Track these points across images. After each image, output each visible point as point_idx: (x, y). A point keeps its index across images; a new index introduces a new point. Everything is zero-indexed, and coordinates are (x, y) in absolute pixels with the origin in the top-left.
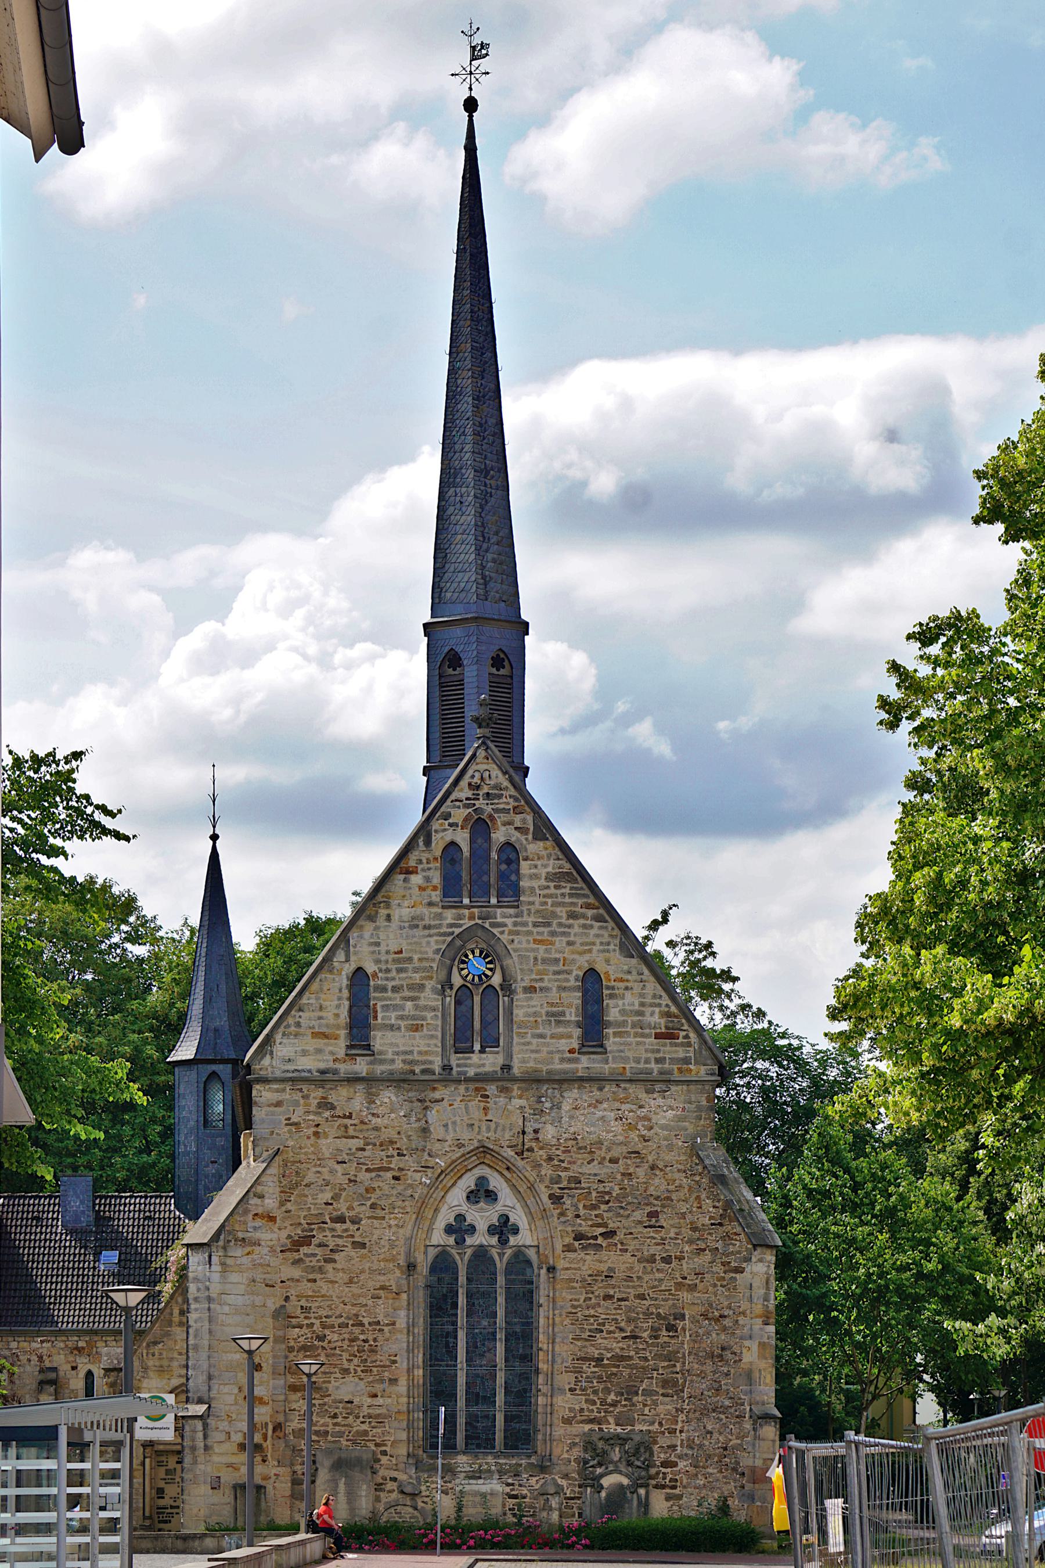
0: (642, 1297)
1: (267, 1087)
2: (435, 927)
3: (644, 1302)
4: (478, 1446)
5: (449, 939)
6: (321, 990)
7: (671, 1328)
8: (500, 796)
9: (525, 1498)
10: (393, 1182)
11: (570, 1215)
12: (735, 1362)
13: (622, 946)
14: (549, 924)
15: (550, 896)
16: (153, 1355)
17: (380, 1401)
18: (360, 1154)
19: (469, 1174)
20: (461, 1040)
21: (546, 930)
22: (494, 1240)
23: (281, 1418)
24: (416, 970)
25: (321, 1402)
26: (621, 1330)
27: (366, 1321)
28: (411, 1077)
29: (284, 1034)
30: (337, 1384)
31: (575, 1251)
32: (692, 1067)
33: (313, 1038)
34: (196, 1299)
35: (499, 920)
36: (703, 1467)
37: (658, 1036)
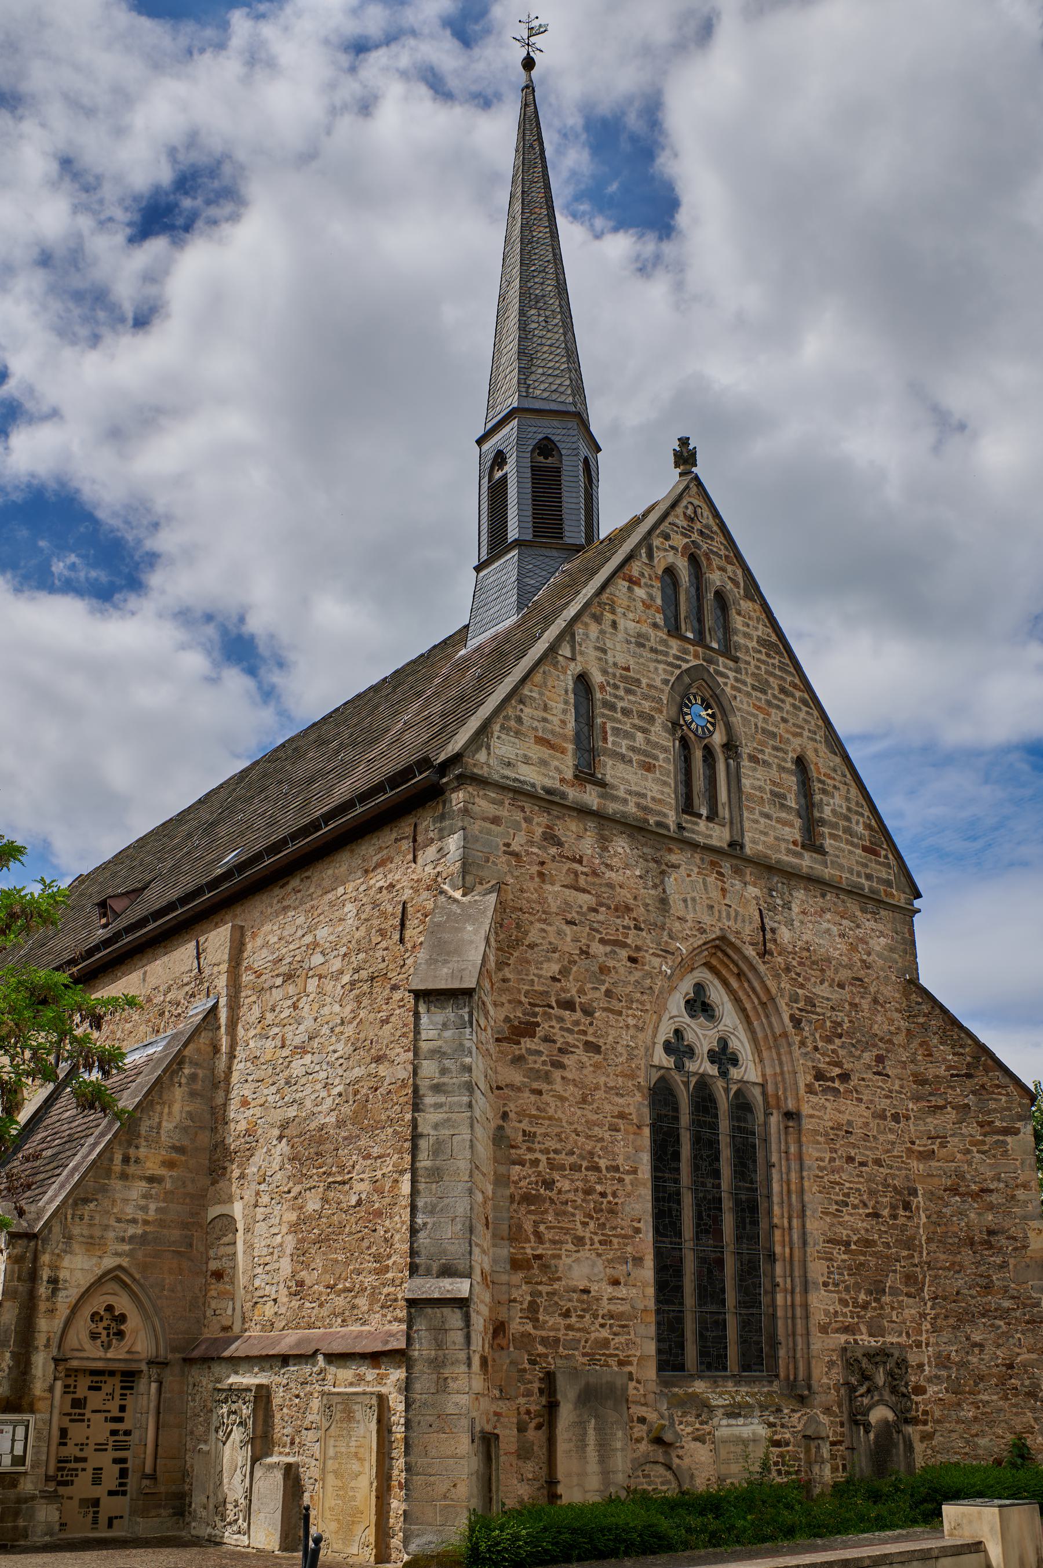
1: (481, 793)
2: (661, 652)
3: (881, 1170)
5: (677, 672)
6: (545, 683)
9: (787, 1444)
10: (629, 964)
12: (1015, 1249)
16: (81, 1219)
17: (622, 1292)
18: (592, 916)
24: (645, 697)
25: (549, 1288)
26: (865, 1205)
27: (603, 1163)
29: (502, 727)
30: (569, 1261)
31: (816, 1094)
33: (536, 743)
34: (437, 1088)
35: (721, 669)
36: (970, 1393)
37: (865, 849)
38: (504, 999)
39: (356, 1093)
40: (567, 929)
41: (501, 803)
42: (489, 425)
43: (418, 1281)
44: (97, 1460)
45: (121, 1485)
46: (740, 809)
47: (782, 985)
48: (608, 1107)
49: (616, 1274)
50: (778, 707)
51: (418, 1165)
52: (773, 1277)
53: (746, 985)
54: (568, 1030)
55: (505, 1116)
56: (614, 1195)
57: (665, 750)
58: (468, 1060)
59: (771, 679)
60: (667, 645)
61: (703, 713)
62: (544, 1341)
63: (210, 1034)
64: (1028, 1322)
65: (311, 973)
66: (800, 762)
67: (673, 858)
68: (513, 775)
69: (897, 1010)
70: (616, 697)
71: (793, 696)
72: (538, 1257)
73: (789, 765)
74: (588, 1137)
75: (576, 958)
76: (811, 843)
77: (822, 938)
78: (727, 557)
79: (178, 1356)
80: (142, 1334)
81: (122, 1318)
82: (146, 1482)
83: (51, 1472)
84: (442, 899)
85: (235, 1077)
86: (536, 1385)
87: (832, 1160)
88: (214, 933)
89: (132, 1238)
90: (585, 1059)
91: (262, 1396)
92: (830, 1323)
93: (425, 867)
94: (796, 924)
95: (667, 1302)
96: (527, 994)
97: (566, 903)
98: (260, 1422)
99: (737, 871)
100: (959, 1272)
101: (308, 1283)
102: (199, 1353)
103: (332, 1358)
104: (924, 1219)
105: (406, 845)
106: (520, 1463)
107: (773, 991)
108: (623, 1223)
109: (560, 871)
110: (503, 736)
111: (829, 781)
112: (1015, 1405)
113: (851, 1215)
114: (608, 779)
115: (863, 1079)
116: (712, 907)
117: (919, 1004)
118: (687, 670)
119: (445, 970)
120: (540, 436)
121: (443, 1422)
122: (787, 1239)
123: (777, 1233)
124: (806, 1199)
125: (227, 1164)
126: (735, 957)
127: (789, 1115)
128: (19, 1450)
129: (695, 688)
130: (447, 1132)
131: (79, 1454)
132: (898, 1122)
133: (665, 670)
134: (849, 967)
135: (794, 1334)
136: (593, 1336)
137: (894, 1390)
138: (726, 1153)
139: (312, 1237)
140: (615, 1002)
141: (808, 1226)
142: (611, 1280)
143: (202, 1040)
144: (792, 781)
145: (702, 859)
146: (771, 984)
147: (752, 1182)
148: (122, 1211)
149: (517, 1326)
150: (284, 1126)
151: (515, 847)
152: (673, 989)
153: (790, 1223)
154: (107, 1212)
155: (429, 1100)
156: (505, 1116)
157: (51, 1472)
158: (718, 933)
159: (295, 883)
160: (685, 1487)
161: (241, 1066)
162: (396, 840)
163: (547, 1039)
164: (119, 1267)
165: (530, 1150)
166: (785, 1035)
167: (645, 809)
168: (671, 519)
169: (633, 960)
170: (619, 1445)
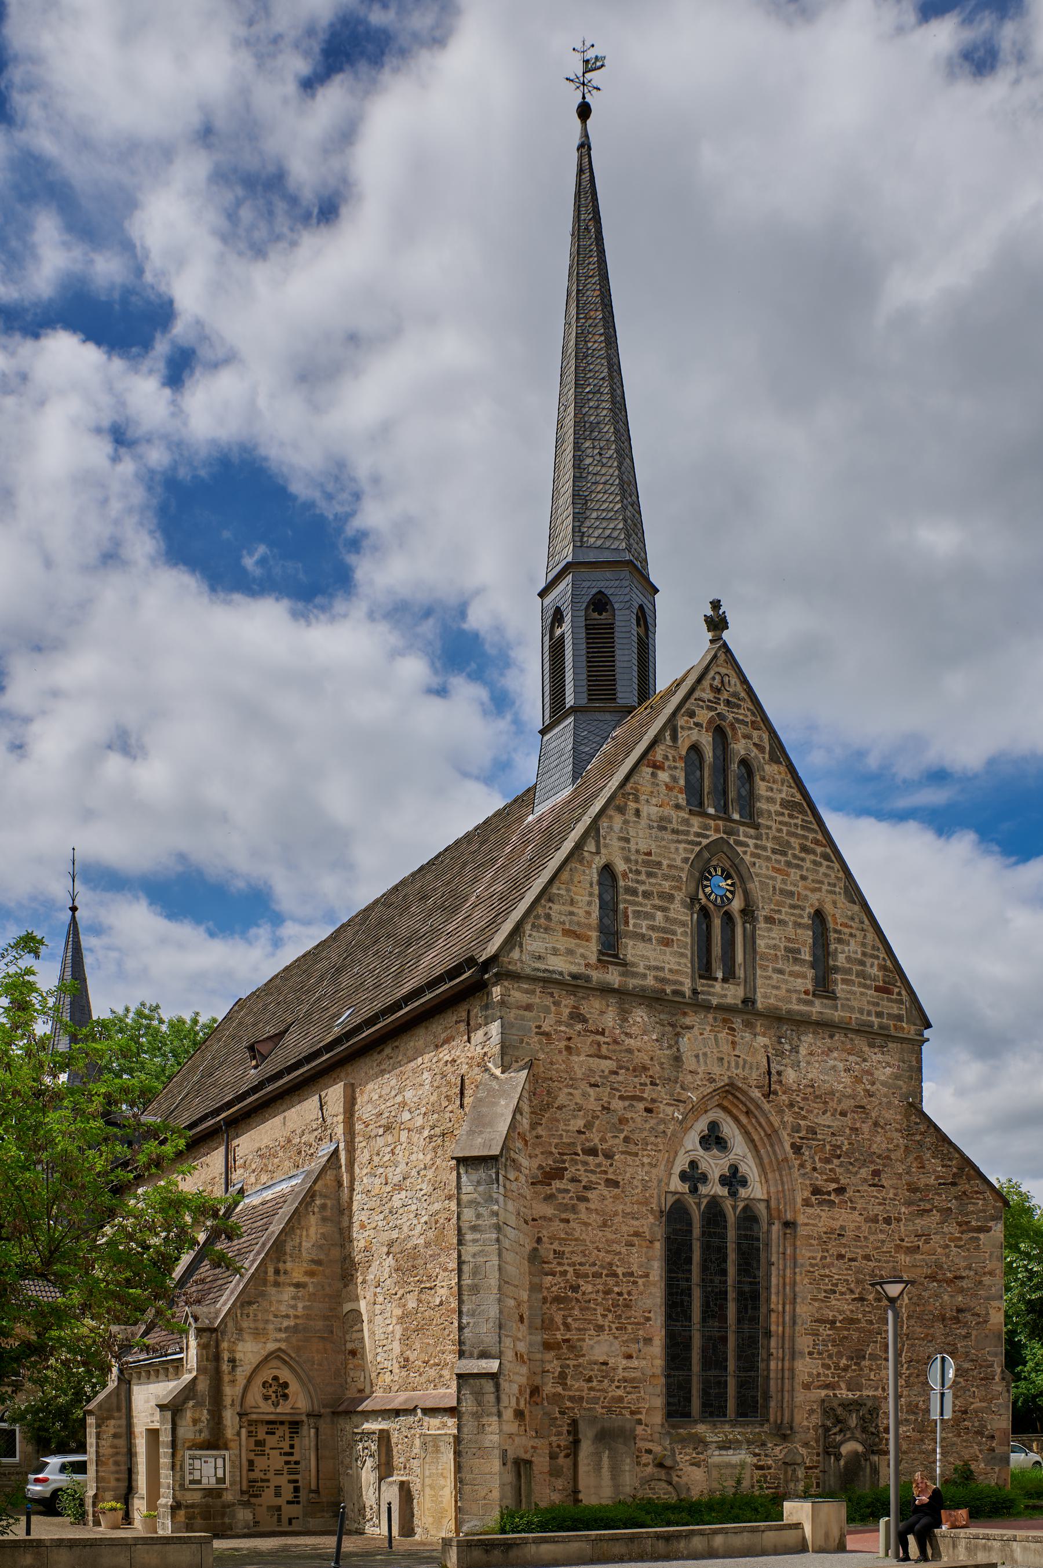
1: (516, 986)
3: (870, 1263)
5: (697, 849)
9: (769, 1468)
10: (645, 1114)
12: (978, 1323)
16: (248, 1316)
17: (635, 1363)
24: (666, 877)
25: (575, 1362)
26: (852, 1292)
27: (620, 1271)
29: (533, 926)
30: (591, 1342)
31: (812, 1206)
32: (905, 1025)
33: (564, 935)
34: (474, 1228)
35: (742, 838)
37: (878, 989)
38: (538, 1151)
39: (436, 1222)
40: (591, 1091)
41: (533, 992)
42: (550, 577)
43: (464, 1362)
45: (295, 1497)
46: (754, 968)
47: (785, 1119)
48: (624, 1228)
49: (629, 1351)
50: (798, 867)
51: (462, 1283)
52: (769, 1349)
53: (754, 1121)
55: (539, 1240)
56: (629, 1293)
57: (683, 924)
58: (496, 1207)
59: (792, 840)
61: (723, 884)
62: (571, 1399)
63: (335, 1172)
64: (982, 1379)
65: (402, 1127)
66: (819, 916)
67: (688, 1021)
68: (543, 967)
69: (897, 1130)
70: (638, 882)
71: (814, 853)
72: (567, 1341)
73: (806, 920)
74: (608, 1252)
75: (599, 1113)
76: (823, 987)
77: (827, 1074)
78: (753, 722)
79: (328, 1410)
80: (301, 1396)
81: (285, 1385)
82: (312, 1495)
83: (244, 1488)
84: (487, 1076)
85: (355, 1207)
86: (565, 1428)
87: (823, 1258)
88: (331, 1089)
89: (287, 1328)
90: (605, 1193)
91: (384, 1437)
92: (813, 1382)
93: (475, 1050)
94: (803, 1064)
95: (677, 1369)
96: (556, 1146)
97: (590, 1070)
98: (383, 1455)
99: (748, 1025)
100: (931, 1341)
101: (411, 1359)
102: (342, 1406)
103: (426, 1411)
104: (906, 1301)
105: (462, 1027)
106: (553, 1479)
107: (776, 1125)
108: (636, 1314)
109: (585, 1044)
110: (534, 934)
111: (846, 930)
112: (965, 1441)
113: (838, 1300)
114: (629, 958)
115: (858, 1191)
116: (722, 1059)
117: (917, 1124)
118: (707, 846)
119: (480, 1140)
120: (594, 591)
121: (482, 1451)
122: (781, 1320)
123: (773, 1316)
124: (797, 1289)
125: (354, 1272)
126: (744, 1099)
127: (787, 1224)
128: (220, 1474)
129: (714, 860)
130: (482, 1260)
131: (264, 1477)
132: (889, 1224)
133: (685, 849)
134: (853, 1097)
135: (782, 1391)
136: (610, 1394)
137: (864, 1430)
138: (732, 1256)
139: (413, 1327)
140: (632, 1146)
141: (798, 1310)
142: (629, 1357)
143: (328, 1177)
144: (807, 936)
145: (715, 1019)
146: (775, 1120)
147: (755, 1278)
148: (278, 1309)
149: (549, 1388)
150: (390, 1245)
151: (546, 1028)
152: (686, 1130)
153: (784, 1308)
154: (267, 1311)
155: (469, 1237)
156: (539, 1240)
157: (244, 1488)
158: (727, 1081)
159: (388, 1051)
160: (682, 1497)
161: (359, 1197)
162: (457, 1022)
163: (574, 1180)
164: (280, 1349)
165: (559, 1264)
166: (785, 1160)
167: (663, 980)
168: (697, 694)
169: (648, 1110)
170: (627, 1468)
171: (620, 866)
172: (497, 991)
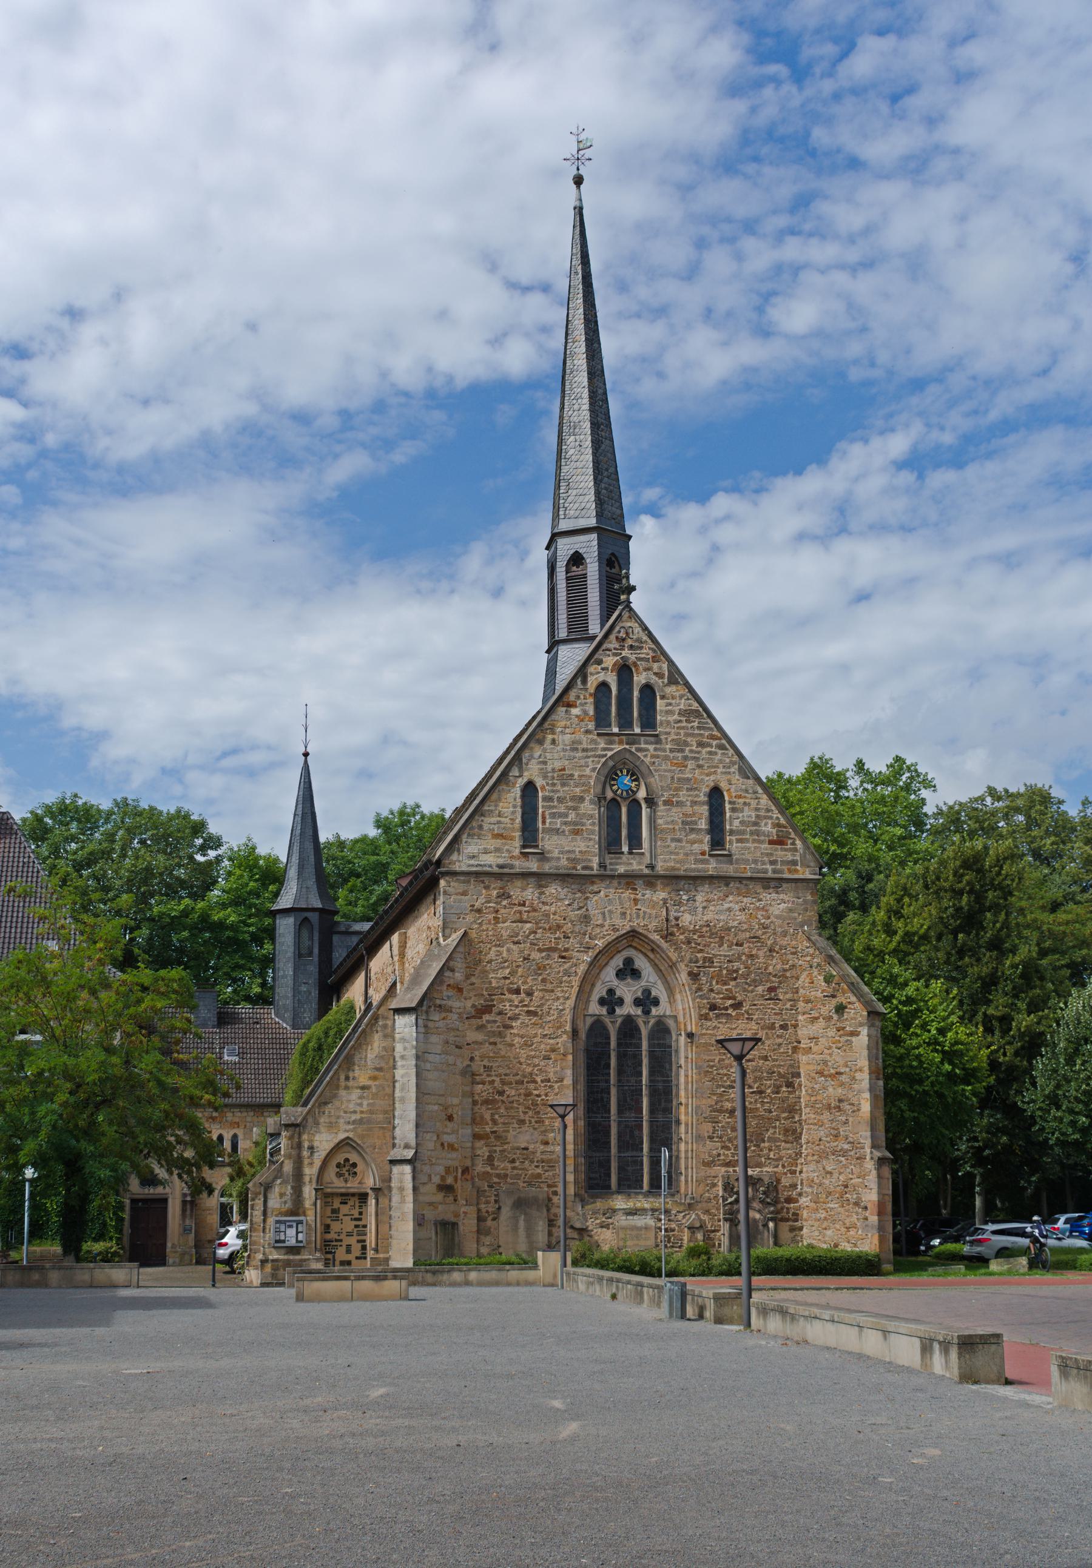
0: (765, 1058)
2: (592, 750)
4: (629, 1187)
5: (604, 760)
7: (790, 1085)
8: (641, 648)
9: (673, 1230)
11: (706, 988)
13: (740, 769)
14: (683, 751)
15: (683, 728)
19: (619, 955)
20: (611, 845)
21: (680, 755)
22: (639, 1011)
23: (468, 1163)
27: (539, 1079)
28: (574, 872)
29: (469, 835)
32: (798, 868)
34: (403, 1057)
35: (643, 746)
37: (771, 842)
40: (514, 947)
44: (348, 1241)
54: (517, 1006)
55: (472, 1059)
60: (596, 743)
62: (498, 1176)
66: (716, 794)
72: (495, 1132)
89: (354, 1122)
120: (572, 552)
149: (480, 1168)
164: (348, 1138)
165: (488, 1075)
171: (539, 782)
172: (442, 883)
